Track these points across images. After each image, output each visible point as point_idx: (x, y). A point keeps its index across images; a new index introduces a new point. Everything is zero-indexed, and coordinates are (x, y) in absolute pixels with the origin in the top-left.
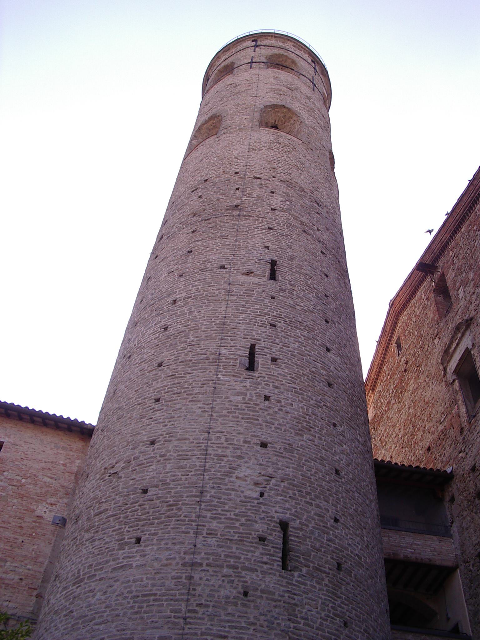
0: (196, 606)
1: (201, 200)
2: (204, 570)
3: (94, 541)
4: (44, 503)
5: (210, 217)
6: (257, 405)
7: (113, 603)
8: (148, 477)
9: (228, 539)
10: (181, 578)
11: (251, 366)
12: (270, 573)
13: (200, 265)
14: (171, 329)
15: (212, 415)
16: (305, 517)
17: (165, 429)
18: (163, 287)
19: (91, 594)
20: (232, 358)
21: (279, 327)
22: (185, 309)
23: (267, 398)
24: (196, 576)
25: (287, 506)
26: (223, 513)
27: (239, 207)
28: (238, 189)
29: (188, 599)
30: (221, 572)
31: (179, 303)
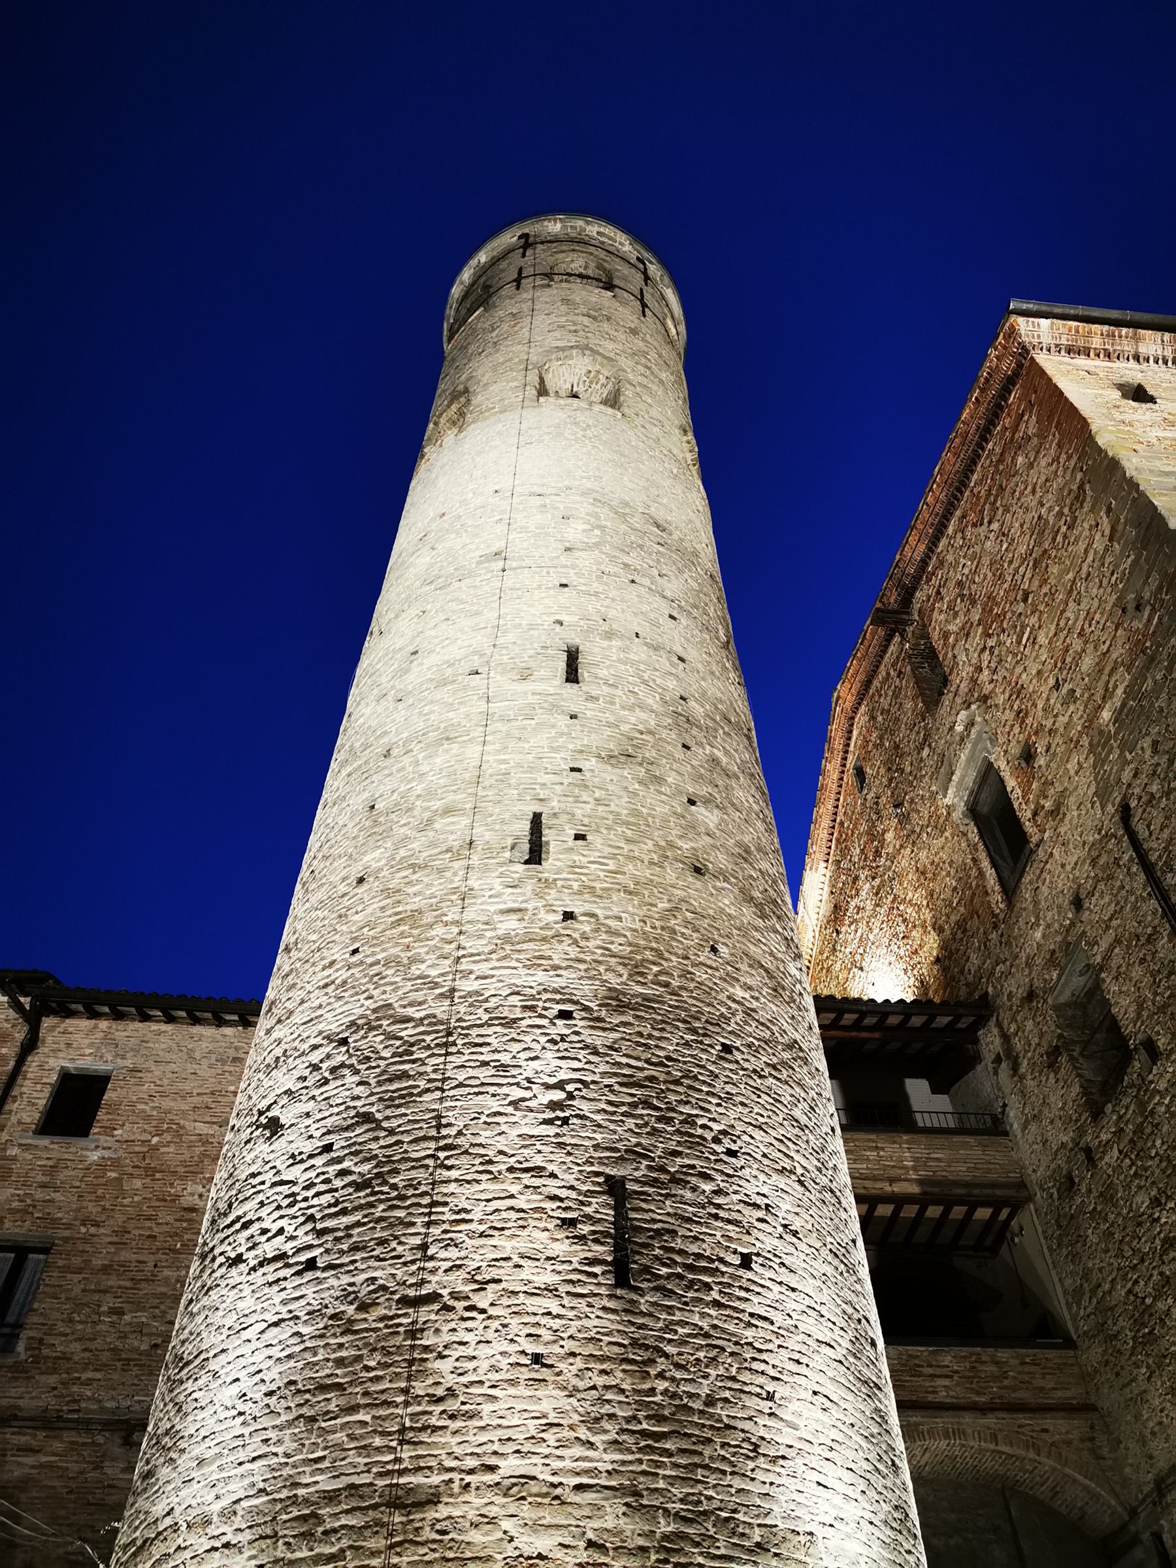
11: (536, 854)
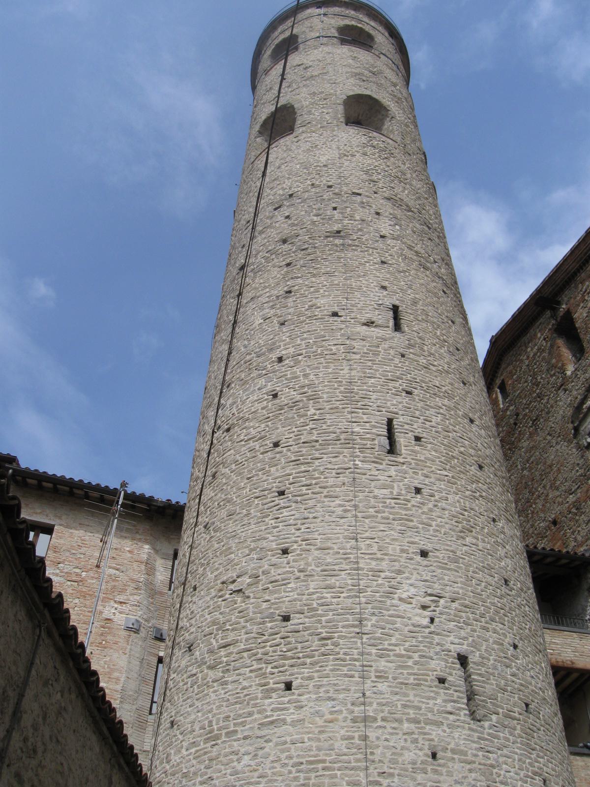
0: (379, 776)
1: (290, 222)
2: (380, 727)
3: (226, 683)
4: (112, 603)
5: (306, 246)
6: (408, 501)
7: (269, 772)
8: (287, 599)
9: (402, 683)
10: (353, 738)
12: (458, 726)
13: (306, 311)
14: (283, 396)
15: (356, 516)
16: (484, 647)
17: (298, 533)
18: (260, 338)
19: (235, 757)
20: (368, 438)
21: (417, 395)
22: (297, 370)
23: (418, 491)
24: (372, 735)
25: (463, 633)
26: (391, 647)
27: (342, 234)
28: (335, 209)
29: (367, 766)
30: (402, 730)
31: (287, 362)
